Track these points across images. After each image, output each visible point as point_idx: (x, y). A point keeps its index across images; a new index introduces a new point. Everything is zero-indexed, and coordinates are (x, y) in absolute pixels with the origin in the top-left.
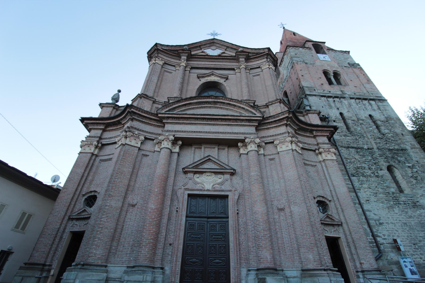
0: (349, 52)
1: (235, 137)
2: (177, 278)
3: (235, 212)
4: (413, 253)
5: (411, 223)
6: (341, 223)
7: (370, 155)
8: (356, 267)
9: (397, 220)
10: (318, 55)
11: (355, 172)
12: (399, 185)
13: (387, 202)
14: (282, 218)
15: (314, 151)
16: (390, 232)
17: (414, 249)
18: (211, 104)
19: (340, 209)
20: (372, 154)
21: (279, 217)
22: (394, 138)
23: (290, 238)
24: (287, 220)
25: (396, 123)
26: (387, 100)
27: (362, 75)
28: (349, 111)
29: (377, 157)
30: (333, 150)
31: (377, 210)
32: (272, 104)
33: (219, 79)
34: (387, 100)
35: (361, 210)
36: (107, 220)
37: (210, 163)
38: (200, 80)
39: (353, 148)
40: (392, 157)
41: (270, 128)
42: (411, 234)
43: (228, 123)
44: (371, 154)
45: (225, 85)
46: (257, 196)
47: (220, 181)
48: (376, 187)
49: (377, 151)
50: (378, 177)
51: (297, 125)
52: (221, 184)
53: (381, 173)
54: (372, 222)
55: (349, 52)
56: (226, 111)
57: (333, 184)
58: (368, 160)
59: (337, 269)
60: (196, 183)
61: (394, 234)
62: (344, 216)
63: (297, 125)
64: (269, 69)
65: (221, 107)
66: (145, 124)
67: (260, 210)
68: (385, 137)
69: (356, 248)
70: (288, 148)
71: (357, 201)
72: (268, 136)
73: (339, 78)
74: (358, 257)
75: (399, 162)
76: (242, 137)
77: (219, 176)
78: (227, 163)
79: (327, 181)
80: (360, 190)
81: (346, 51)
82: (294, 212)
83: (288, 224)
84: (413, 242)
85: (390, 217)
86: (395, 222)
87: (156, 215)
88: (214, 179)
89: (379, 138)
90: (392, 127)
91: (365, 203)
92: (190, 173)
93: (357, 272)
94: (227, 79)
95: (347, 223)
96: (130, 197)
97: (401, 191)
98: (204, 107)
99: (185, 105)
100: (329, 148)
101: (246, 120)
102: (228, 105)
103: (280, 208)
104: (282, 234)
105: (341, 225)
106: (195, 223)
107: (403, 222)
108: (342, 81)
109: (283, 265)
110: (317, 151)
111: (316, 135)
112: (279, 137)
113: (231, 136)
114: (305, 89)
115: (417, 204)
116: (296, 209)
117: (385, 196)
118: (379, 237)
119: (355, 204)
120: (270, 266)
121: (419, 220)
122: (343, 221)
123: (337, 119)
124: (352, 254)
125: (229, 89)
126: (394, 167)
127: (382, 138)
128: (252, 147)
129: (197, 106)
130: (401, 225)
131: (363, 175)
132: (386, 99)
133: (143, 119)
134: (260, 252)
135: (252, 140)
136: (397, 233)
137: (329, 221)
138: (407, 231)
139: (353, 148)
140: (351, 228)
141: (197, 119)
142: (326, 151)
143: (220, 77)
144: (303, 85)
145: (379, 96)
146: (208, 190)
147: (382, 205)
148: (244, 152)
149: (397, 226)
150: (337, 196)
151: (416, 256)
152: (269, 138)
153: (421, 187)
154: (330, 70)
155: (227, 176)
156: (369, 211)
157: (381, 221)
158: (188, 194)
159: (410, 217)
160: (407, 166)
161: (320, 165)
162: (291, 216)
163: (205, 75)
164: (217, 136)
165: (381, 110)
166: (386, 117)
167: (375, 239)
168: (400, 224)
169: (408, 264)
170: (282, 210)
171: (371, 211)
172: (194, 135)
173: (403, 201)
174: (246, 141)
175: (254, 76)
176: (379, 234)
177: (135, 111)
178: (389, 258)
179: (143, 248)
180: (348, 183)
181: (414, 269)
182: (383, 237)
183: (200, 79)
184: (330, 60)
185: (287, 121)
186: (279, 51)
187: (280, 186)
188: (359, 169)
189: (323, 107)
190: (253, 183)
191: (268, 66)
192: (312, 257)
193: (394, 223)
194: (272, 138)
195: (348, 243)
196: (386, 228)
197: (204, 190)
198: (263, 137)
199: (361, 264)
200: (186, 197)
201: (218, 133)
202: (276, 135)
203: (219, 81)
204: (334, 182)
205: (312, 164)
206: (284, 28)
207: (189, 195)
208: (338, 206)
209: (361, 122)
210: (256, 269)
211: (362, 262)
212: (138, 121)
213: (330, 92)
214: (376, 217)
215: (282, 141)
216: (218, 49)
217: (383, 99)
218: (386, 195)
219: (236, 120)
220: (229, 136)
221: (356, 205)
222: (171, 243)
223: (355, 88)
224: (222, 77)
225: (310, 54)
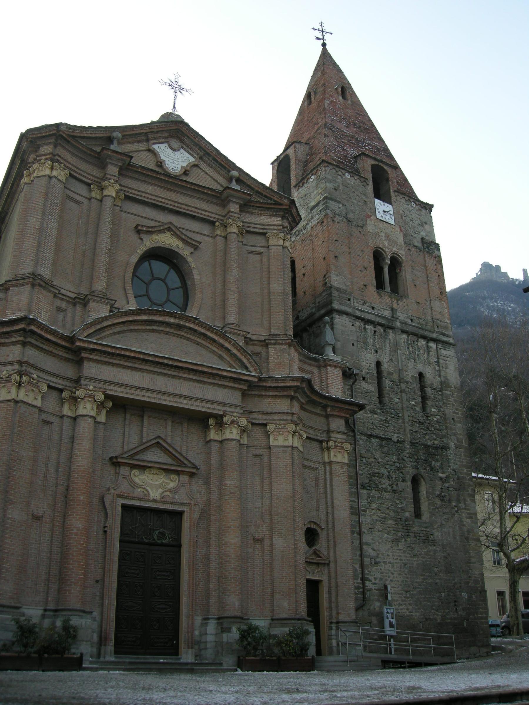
0: (432, 206)
1: (208, 408)
2: (112, 626)
3: (194, 540)
4: (401, 603)
5: (413, 564)
6: (328, 562)
7: (397, 453)
8: (331, 617)
9: (397, 559)
10: (377, 201)
11: (367, 481)
12: (420, 505)
13: (394, 532)
14: (257, 552)
15: (321, 442)
16: (384, 574)
17: (405, 597)
18: (172, 328)
19: (331, 542)
20: (400, 451)
21: (254, 550)
22: (440, 424)
23: (263, 580)
24: (263, 556)
25: (452, 396)
27: (437, 274)
28: (391, 360)
29: (405, 458)
30: (348, 447)
31: (379, 543)
32: (275, 344)
33: (181, 245)
35: (358, 542)
36: (11, 541)
37: (157, 449)
38: (141, 239)
39: (377, 437)
40: (424, 460)
41: (266, 395)
42: (407, 578)
43: (198, 378)
44: (398, 452)
45: (193, 265)
46: (232, 520)
47: (172, 485)
48: (388, 509)
49: (408, 447)
50: (395, 493)
51: (308, 396)
52: (173, 491)
53: (401, 485)
54: (367, 561)
56: (195, 345)
57: (332, 503)
58: (391, 461)
59: (310, 619)
60: (134, 485)
61: (387, 578)
62: (335, 552)
63: (308, 396)
64: (283, 248)
65: (189, 336)
66: (44, 353)
67: (233, 541)
68: (428, 422)
69: (337, 595)
70: (286, 444)
71: (358, 529)
72: (259, 413)
73: (398, 271)
74: (337, 607)
75: (432, 469)
76: (218, 410)
77: (173, 476)
78: (179, 449)
79: (326, 497)
80: (365, 511)
82: (276, 546)
83: (264, 562)
84: (406, 589)
85: (390, 554)
86: (395, 561)
87: (84, 539)
88: (163, 482)
89: (420, 422)
90: (444, 403)
91: (366, 532)
92: (124, 465)
93: (331, 623)
94: (196, 248)
95: (336, 562)
96: (33, 503)
97: (418, 514)
98: (157, 331)
99: (124, 323)
100: (343, 441)
101: (231, 378)
102: (202, 337)
103: (257, 537)
104: (254, 574)
105: (328, 564)
106: (131, 551)
107: (404, 561)
108: (401, 289)
109: (249, 613)
110: (324, 444)
111: (329, 414)
112: (276, 417)
113: (201, 406)
114: (335, 294)
116: (279, 542)
117: (394, 523)
118: (370, 580)
119: (353, 532)
120: (237, 614)
121: (424, 560)
122: (332, 559)
123: (368, 375)
124: (330, 602)
125: (198, 277)
126: (422, 476)
127: (423, 424)
128: (232, 433)
129: (144, 327)
130: (401, 565)
131: (378, 489)
133: (44, 344)
134: (227, 597)
135: (235, 419)
136: (392, 576)
137: (315, 559)
138: (404, 575)
139: (377, 437)
140: (338, 568)
141: (146, 361)
142: (338, 446)
143: (183, 240)
144: (333, 283)
146: (154, 501)
147: (387, 537)
148: (217, 438)
149: (395, 567)
150: (333, 522)
151: (404, 606)
152: (260, 416)
153: (444, 513)
154: (387, 250)
155: (185, 478)
156: (368, 544)
157: (378, 560)
158: (122, 504)
159: (415, 555)
161: (323, 469)
162: (271, 551)
163: (153, 230)
164: (177, 402)
165: (439, 366)
166: (441, 383)
167: (363, 583)
169: (389, 615)
170: (260, 541)
171: (370, 545)
172: (137, 395)
173: (414, 533)
174: (225, 419)
175: (250, 252)
176: (370, 577)
177: (36, 330)
178: (372, 608)
179: (73, 586)
180: (353, 499)
181: (394, 621)
182: (374, 581)
183: (142, 235)
184: (393, 222)
185: (295, 392)
187: (262, 504)
188: (374, 476)
189: (353, 345)
190: (227, 497)
192: (287, 605)
193: (393, 563)
194: (265, 417)
195: (330, 588)
196: (381, 569)
197: (149, 501)
198: (251, 412)
199: (338, 613)
200: (120, 509)
201: (181, 396)
202: (271, 413)
203: (180, 252)
204: (335, 501)
205: (312, 466)
206: (324, 45)
207: (124, 506)
208: (331, 538)
209: (403, 386)
210: (216, 617)
211: (340, 611)
212: (35, 348)
213: (373, 308)
214: (373, 554)
215: (280, 427)
216: (185, 150)
218: (396, 521)
219: (214, 375)
220: (197, 406)
221: (353, 534)
222: (99, 579)
224: (187, 242)
225: (363, 197)
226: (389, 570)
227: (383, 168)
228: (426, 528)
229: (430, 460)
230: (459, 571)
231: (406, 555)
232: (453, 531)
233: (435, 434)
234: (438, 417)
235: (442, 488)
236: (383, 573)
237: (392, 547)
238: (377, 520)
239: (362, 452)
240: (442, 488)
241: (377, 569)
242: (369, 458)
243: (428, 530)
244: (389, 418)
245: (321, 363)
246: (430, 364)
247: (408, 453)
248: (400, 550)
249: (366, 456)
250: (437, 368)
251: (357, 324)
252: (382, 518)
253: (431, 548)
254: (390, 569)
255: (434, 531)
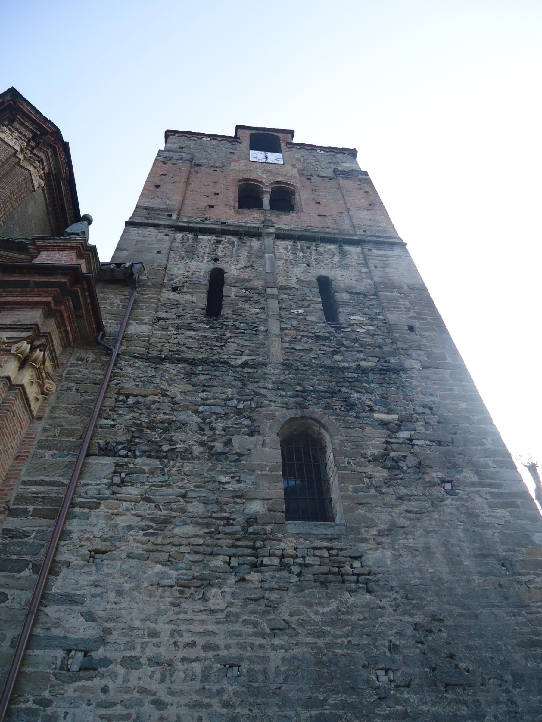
5: (265, 659)
7: (238, 384)
9: (193, 644)
22: (376, 337)
26: (405, 244)
28: (251, 266)
31: (120, 593)
34: (406, 244)
48: (184, 496)
55: (353, 153)
75: (350, 406)
81: (344, 149)
89: (317, 336)
90: (383, 308)
91: (76, 561)
107: (223, 653)
115: (347, 569)
123: (186, 285)
132: (405, 241)
145: (388, 235)
157: (99, 653)
159: (275, 631)
160: (376, 420)
165: (368, 268)
168: (197, 667)
171: (81, 603)
186: (163, 149)
191: (18, 148)
196: (105, 690)
217: (396, 240)
223: (319, 218)
226: (144, 691)
227: (274, 135)
228: (329, 540)
229: (344, 390)
230: (500, 677)
231: (237, 627)
232: (445, 543)
233: (362, 351)
234: (371, 327)
235: (387, 442)
236: (113, 704)
237: (174, 605)
238: (130, 528)
239: (126, 386)
240: (387, 442)
241: (85, 689)
242: (144, 396)
243: (337, 544)
244: (228, 334)
245: (31, 251)
246: (347, 267)
247: (273, 383)
248: (212, 612)
249: (135, 392)
250: (364, 270)
251: (179, 235)
252: (152, 520)
253: (351, 599)
254: (154, 686)
255: (363, 546)
